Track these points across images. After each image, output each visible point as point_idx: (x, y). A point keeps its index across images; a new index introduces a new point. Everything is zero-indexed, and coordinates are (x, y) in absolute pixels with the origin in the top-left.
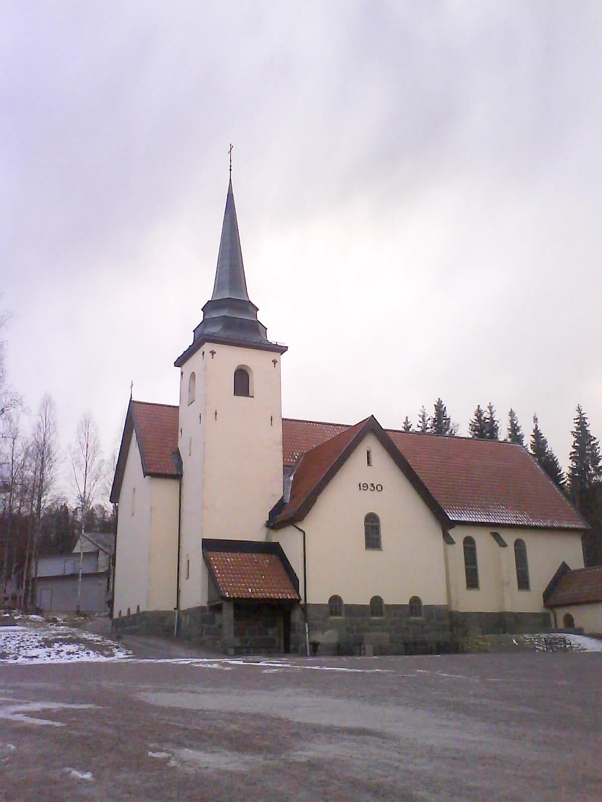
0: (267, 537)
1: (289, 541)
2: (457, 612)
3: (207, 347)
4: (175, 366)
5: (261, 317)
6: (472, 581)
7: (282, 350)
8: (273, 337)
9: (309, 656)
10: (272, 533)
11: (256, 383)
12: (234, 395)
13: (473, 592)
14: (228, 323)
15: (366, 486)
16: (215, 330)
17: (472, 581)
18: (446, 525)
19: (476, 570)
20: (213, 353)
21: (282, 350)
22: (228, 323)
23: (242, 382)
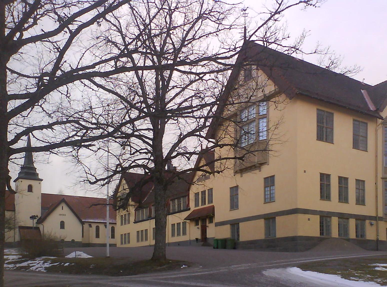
0: (36, 226)
1: (41, 227)
2: (91, 243)
3: (20, 180)
4: (364, 181)
5: (37, 172)
6: (98, 236)
7: (42, 180)
8: (40, 177)
9: (219, 240)
10: (38, 225)
11: (34, 189)
12: (230, 188)
13: (97, 239)
14: (27, 173)
15: (63, 213)
16: (21, 175)
17: (98, 236)
18: (83, 223)
19: (99, 234)
20: (21, 181)
21: (42, 180)
22: (27, 173)
23: (30, 189)
